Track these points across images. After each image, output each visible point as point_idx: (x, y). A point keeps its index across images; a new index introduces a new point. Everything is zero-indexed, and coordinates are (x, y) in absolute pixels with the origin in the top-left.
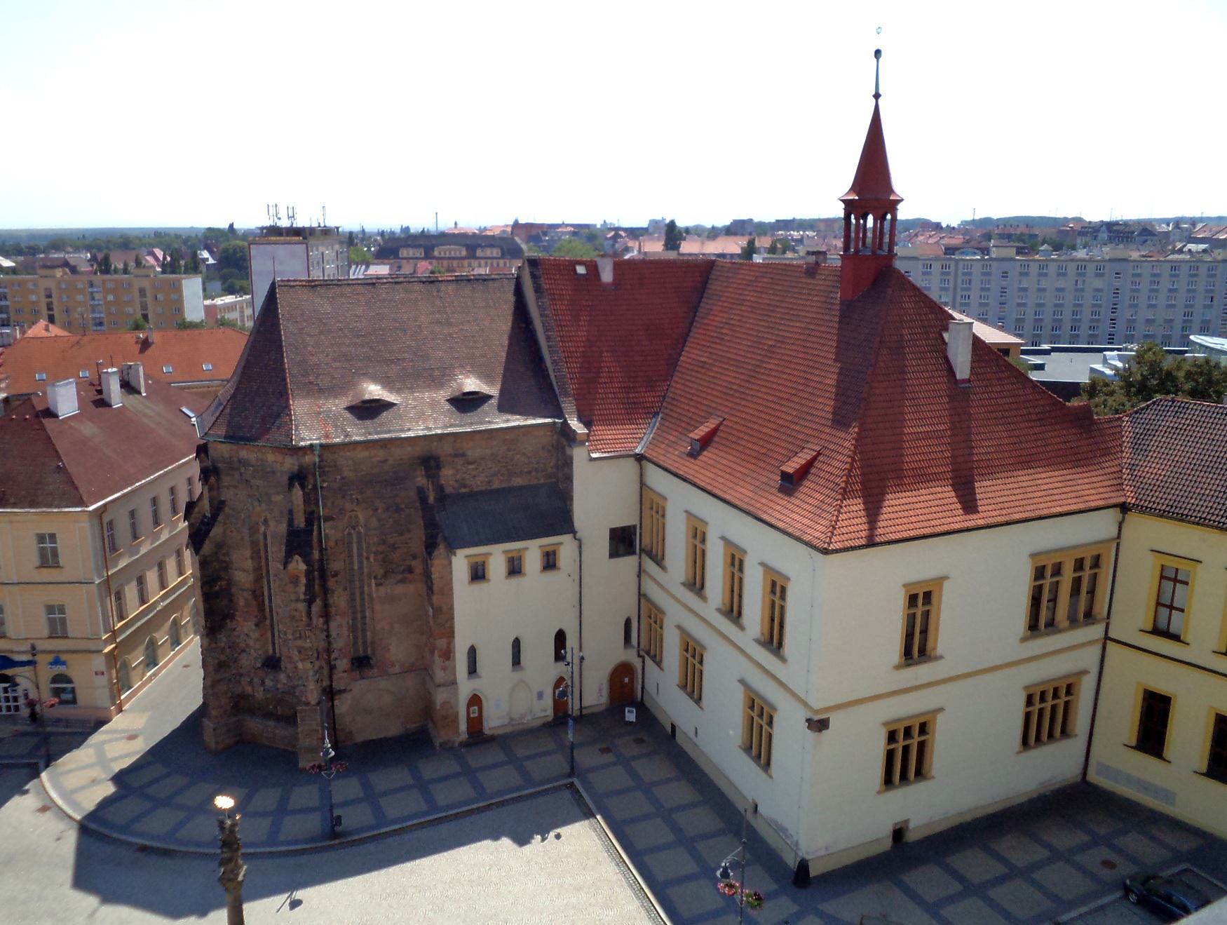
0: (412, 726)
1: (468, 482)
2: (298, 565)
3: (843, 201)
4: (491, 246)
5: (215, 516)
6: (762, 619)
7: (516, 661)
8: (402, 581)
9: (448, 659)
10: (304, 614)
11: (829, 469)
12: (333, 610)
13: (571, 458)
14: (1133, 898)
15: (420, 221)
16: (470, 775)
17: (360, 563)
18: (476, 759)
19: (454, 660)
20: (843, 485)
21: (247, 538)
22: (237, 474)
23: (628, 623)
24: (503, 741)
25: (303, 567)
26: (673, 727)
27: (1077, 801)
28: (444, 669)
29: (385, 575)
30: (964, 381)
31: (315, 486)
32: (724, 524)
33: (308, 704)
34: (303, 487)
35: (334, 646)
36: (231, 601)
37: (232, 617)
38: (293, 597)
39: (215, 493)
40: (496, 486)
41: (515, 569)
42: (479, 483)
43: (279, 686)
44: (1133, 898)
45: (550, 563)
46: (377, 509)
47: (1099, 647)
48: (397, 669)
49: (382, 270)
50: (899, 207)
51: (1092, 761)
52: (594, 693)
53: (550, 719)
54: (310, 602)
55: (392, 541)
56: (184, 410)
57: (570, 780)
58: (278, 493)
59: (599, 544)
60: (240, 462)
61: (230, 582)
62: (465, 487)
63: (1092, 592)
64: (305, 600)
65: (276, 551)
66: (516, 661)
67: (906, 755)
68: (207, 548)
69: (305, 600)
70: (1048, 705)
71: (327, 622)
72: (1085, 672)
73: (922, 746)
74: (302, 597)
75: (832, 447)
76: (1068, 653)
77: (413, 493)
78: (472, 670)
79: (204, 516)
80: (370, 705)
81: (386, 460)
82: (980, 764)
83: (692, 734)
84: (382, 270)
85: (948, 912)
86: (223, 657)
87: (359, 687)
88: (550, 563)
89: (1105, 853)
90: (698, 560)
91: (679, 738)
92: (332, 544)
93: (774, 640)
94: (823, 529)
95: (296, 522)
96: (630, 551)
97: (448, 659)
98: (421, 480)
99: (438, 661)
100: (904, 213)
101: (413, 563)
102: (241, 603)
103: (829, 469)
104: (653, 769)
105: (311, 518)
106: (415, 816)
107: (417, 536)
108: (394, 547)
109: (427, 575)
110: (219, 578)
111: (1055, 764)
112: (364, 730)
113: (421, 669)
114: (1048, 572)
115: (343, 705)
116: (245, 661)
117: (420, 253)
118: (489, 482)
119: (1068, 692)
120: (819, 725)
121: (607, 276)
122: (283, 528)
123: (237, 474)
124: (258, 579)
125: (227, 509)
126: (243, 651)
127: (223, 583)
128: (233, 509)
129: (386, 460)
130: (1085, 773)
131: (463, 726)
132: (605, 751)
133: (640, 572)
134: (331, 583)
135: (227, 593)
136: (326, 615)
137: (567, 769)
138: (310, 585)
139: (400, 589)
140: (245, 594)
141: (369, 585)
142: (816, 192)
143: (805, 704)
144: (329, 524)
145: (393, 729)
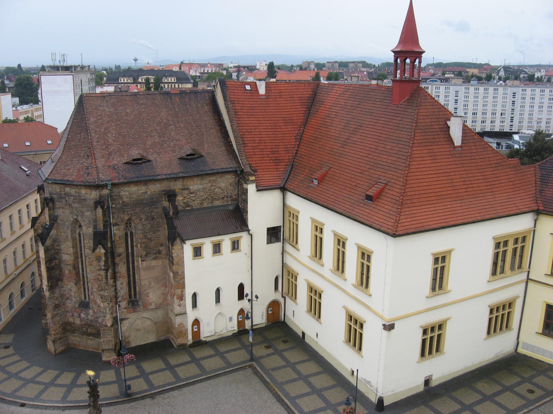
0: (162, 338)
1: (190, 204)
2: (101, 251)
3: (393, 52)
4: (171, 76)
5: (52, 226)
7: (218, 300)
8: (155, 259)
10: (104, 277)
11: (392, 193)
12: (118, 275)
13: (247, 190)
15: (125, 61)
16: (195, 361)
18: (199, 353)
19: (185, 301)
20: (401, 201)
21: (70, 236)
22: (64, 201)
23: (277, 279)
24: (215, 343)
25: (103, 251)
26: (303, 334)
27: (514, 364)
28: (180, 306)
29: (146, 255)
30: (458, 147)
31: (108, 207)
32: (334, 224)
33: (107, 326)
34: (102, 207)
35: (119, 294)
36: (61, 271)
37: (61, 280)
38: (98, 268)
39: (52, 212)
40: (205, 205)
41: (217, 249)
42: (195, 204)
43: (89, 317)
45: (235, 246)
46: (141, 220)
47: (524, 285)
48: (153, 306)
49: (110, 89)
50: (423, 55)
51: (521, 340)
52: (259, 318)
53: (236, 332)
54: (107, 270)
55: (149, 236)
56: (23, 167)
57: (250, 363)
58: (88, 211)
59: (261, 235)
60: (65, 194)
61: (60, 261)
62: (189, 206)
63: (521, 256)
64: (104, 270)
65: (88, 243)
66: (218, 300)
67: (432, 341)
68: (48, 242)
69: (104, 270)
70: (500, 314)
71: (115, 282)
72: (517, 297)
73: (439, 336)
74: (103, 268)
75: (393, 181)
76: (509, 287)
77: (160, 210)
78: (195, 305)
79: (46, 225)
80: (139, 328)
81: (146, 192)
82: (468, 348)
83: (314, 337)
84: (110, 89)
85: (477, 408)
86: (57, 303)
88: (235, 246)
89: (529, 386)
90: (318, 243)
91: (307, 340)
92: (117, 238)
93: (364, 279)
94: (392, 224)
96: (278, 240)
97: (182, 300)
98: (166, 204)
99: (176, 301)
100: (427, 59)
101: (161, 248)
102: (67, 272)
103: (392, 193)
104: (294, 356)
105: (107, 224)
106: (169, 384)
107: (164, 232)
108: (150, 239)
109: (170, 256)
110: (55, 259)
111: (502, 345)
112: (137, 340)
113: (164, 305)
114: (520, 241)
115: (125, 327)
116: (69, 304)
117: (130, 80)
119: (510, 307)
120: (389, 327)
121: (262, 90)
122: (91, 230)
123: (64, 201)
124: (76, 258)
125: (59, 221)
126: (68, 298)
127: (57, 261)
128: (62, 220)
129: (146, 192)
130: (516, 349)
131: (190, 337)
132: (267, 347)
133: (283, 252)
134: (117, 260)
135: (58, 267)
136: (115, 278)
137: (249, 357)
138: (106, 261)
139: (154, 263)
140: (69, 267)
141: (138, 261)
142: (381, 49)
143: (382, 318)
144: (116, 228)
145: (151, 338)
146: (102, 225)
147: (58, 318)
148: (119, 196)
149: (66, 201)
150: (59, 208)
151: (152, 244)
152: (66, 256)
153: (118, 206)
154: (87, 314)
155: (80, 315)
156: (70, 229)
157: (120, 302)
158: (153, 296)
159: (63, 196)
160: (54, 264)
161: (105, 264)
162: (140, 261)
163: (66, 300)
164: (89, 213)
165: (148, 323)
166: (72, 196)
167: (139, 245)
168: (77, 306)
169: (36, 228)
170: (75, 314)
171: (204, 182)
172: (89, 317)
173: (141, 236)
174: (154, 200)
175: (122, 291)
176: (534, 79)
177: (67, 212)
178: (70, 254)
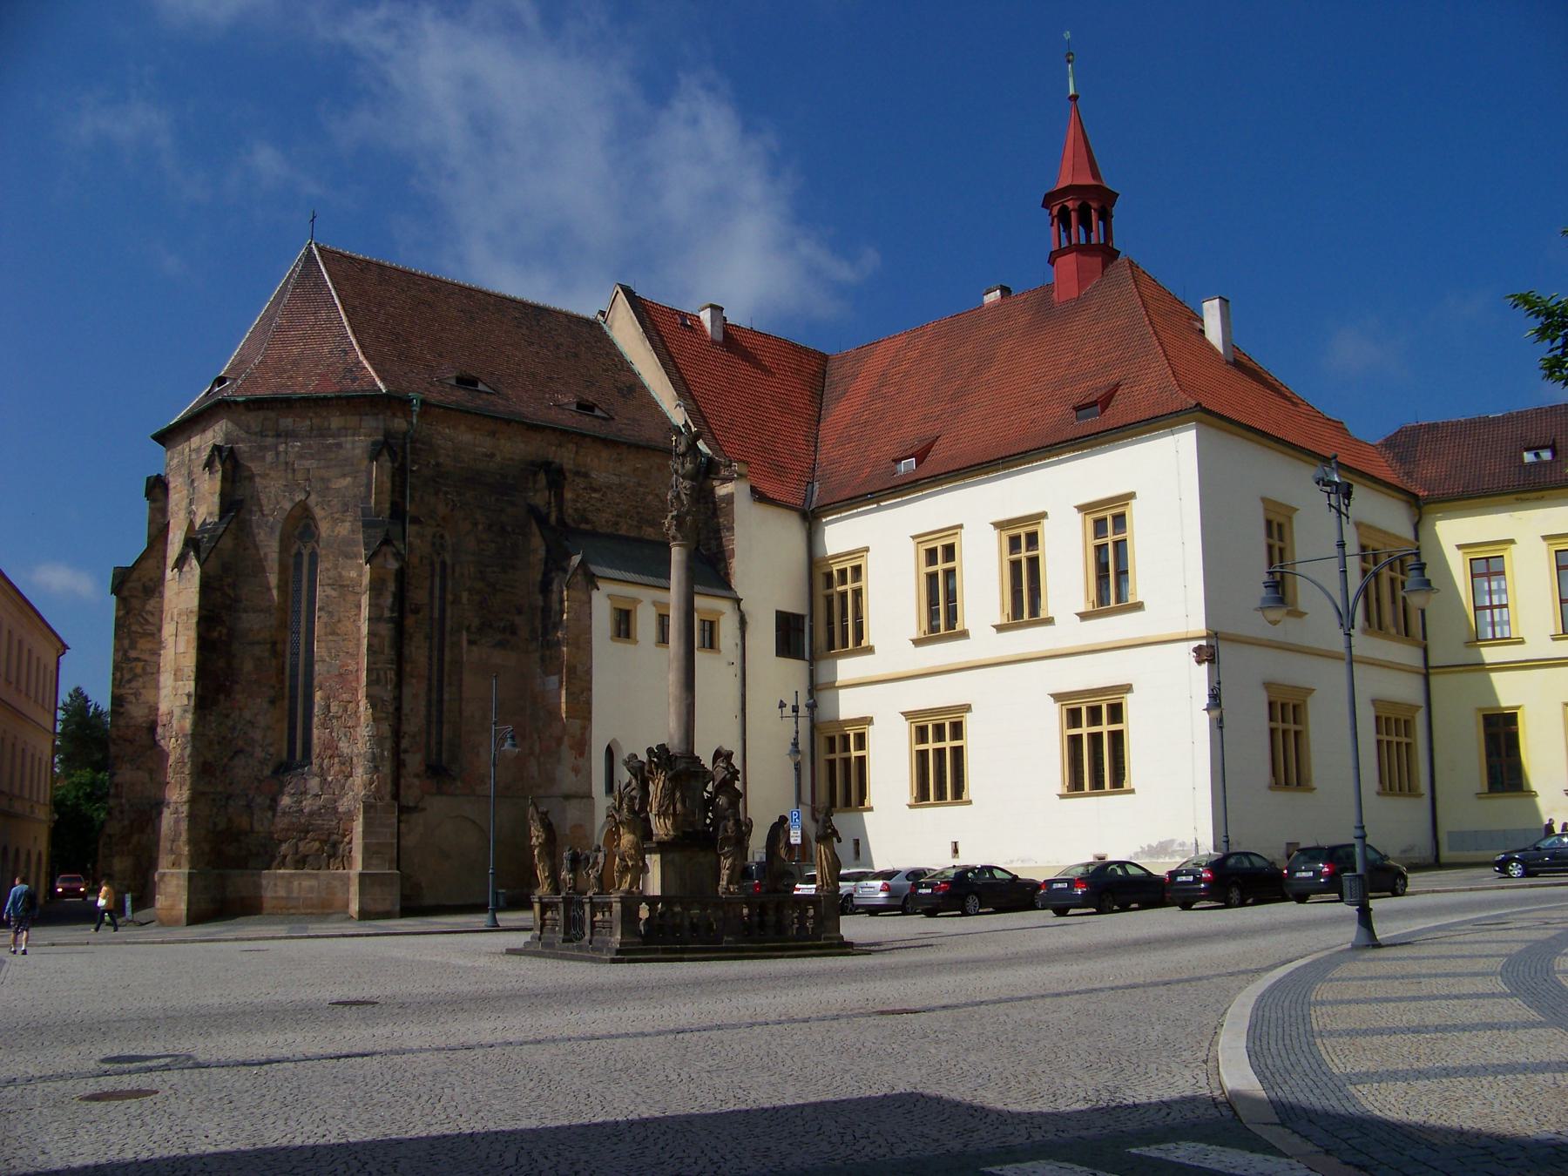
8: (501, 645)
9: (582, 754)
12: (408, 668)
14: (1515, 870)
17: (443, 611)
28: (576, 770)
35: (406, 728)
44: (1515, 870)
46: (476, 524)
51: (1445, 826)
58: (344, 476)
59: (764, 635)
62: (587, 521)
64: (391, 620)
74: (387, 614)
81: (492, 455)
87: (437, 806)
99: (567, 754)
101: (518, 620)
102: (248, 666)
124: (259, 643)
129: (492, 455)
146: (388, 505)
149: (278, 454)
156: (277, 534)
157: (406, 751)
158: (494, 749)
160: (216, 634)
163: (231, 758)
167: (465, 595)
168: (267, 772)
169: (125, 593)
170: (259, 800)
171: (624, 469)
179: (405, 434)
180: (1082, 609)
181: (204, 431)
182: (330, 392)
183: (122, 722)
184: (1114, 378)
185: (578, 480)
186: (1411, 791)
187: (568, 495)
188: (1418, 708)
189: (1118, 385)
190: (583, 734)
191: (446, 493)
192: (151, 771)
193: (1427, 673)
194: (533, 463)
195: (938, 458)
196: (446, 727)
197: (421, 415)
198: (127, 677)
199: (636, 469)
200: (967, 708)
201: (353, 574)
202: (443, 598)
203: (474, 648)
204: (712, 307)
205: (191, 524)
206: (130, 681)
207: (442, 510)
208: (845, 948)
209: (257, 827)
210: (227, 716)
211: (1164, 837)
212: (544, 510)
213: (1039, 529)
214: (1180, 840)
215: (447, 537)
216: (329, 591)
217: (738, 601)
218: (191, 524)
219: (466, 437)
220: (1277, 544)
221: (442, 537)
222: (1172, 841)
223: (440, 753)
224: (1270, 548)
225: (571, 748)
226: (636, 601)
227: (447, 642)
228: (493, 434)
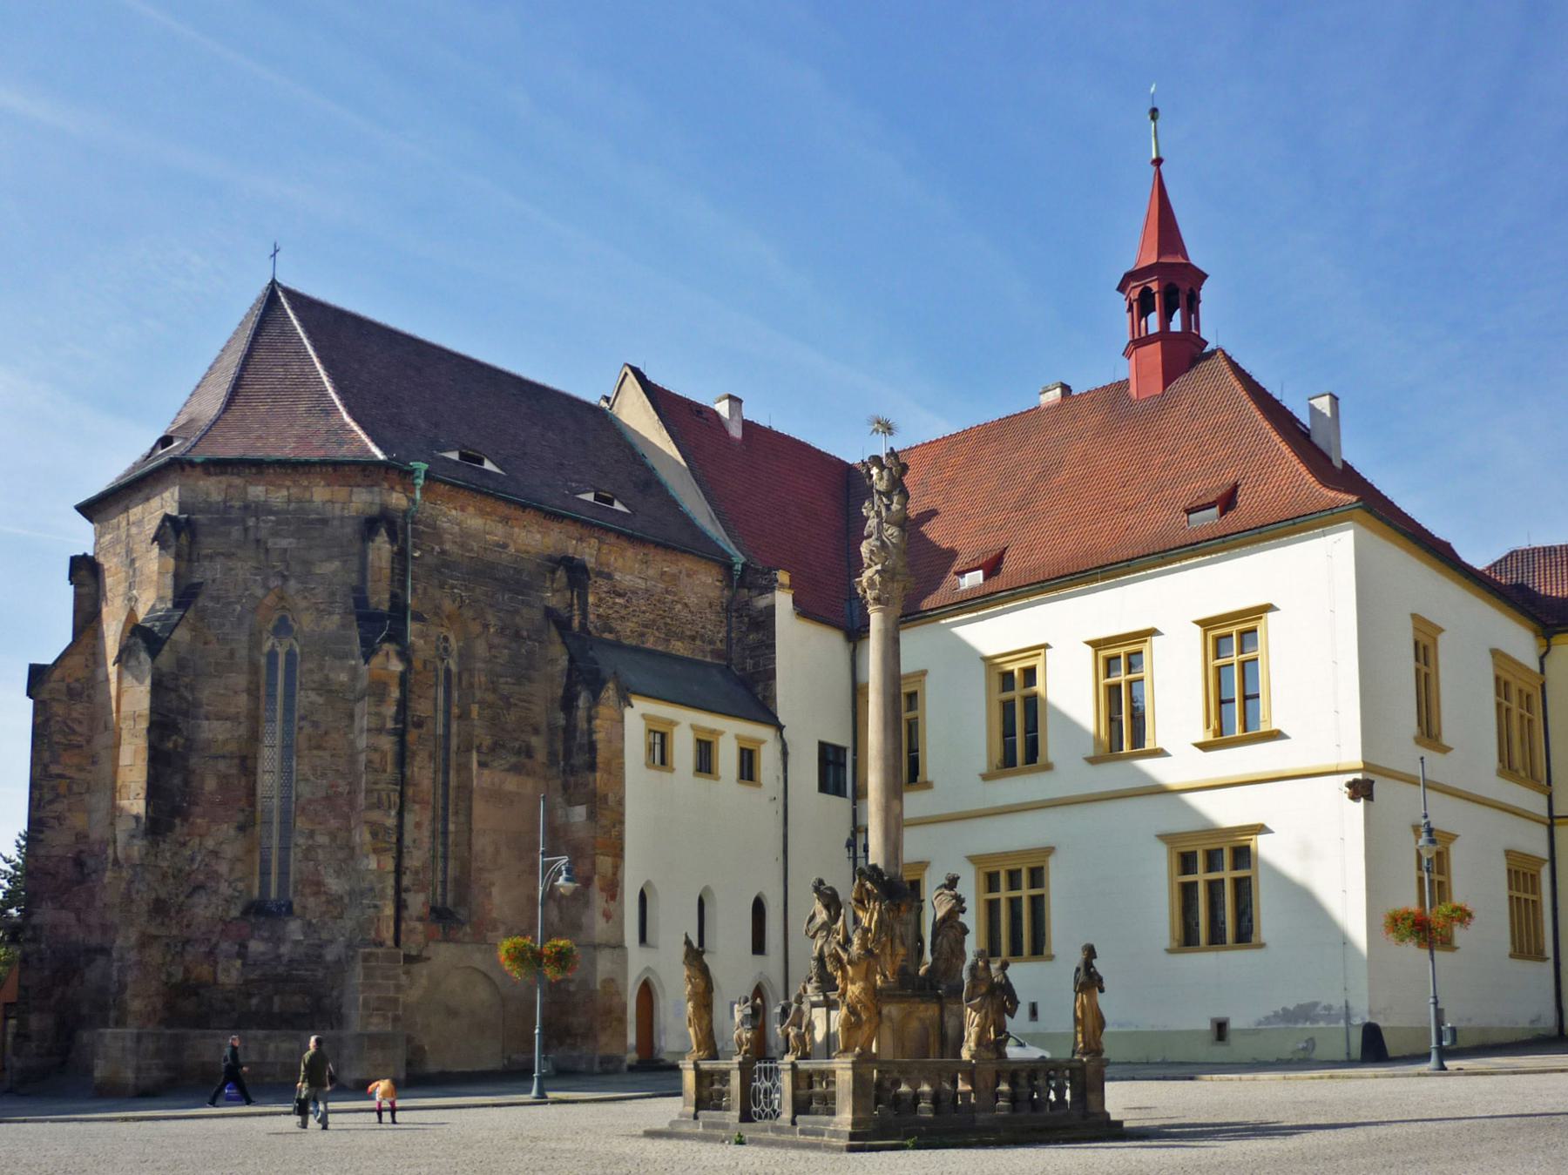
6: (1408, 551)
8: (516, 769)
10: (390, 758)
12: (410, 792)
17: (447, 726)
19: (622, 903)
22: (236, 532)
25: (397, 666)
28: (607, 916)
33: (381, 944)
34: (393, 537)
36: (186, 783)
43: (284, 949)
46: (486, 626)
58: (330, 558)
59: (806, 769)
60: (246, 507)
64: (394, 732)
68: (166, 658)
69: (394, 732)
74: (390, 725)
81: (505, 546)
87: (444, 954)
95: (373, 600)
99: (598, 899)
102: (211, 784)
108: (506, 699)
118: (642, 635)
123: (236, 532)
124: (224, 757)
126: (199, 887)
128: (217, 599)
129: (505, 546)
140: (222, 766)
146: (387, 596)
147: (155, 954)
148: (435, 527)
149: (246, 530)
150: (211, 557)
151: (511, 718)
152: (216, 724)
153: (429, 560)
154: (278, 940)
155: (243, 946)
157: (407, 890)
159: (234, 514)
160: (170, 745)
161: (398, 712)
162: (475, 765)
163: (189, 896)
164: (336, 565)
165: (482, 993)
166: (271, 512)
172: (284, 949)
173: (483, 679)
174: (525, 578)
175: (416, 853)
176: (859, 1055)
177: (243, 568)
178: (234, 718)
179: (405, 513)
180: (1200, 739)
181: (148, 499)
182: (315, 455)
183: (41, 852)
184: (1229, 478)
185: (600, 581)
186: (1539, 956)
187: (591, 599)
188: (1541, 861)
189: (1235, 487)
190: (615, 874)
191: (453, 587)
192: (77, 912)
193: (1551, 821)
194: (550, 559)
195: (1249, 507)
196: (451, 864)
197: (424, 490)
198: (48, 797)
199: (663, 573)
200: (1049, 851)
201: (344, 677)
202: (447, 712)
203: (486, 772)
204: (730, 397)
205: (132, 613)
206: (51, 802)
207: (448, 606)
208: (1114, 1132)
209: (222, 978)
210: (184, 844)
211: (1306, 1000)
212: (564, 613)
213: (1145, 648)
214: (1325, 1003)
215: (452, 639)
216: (313, 696)
217: (780, 728)
218: (132, 613)
219: (474, 522)
220: (1424, 669)
221: (446, 639)
222: (1315, 1004)
223: (444, 895)
224: (1417, 671)
225: (602, 890)
226: (672, 723)
227: (453, 764)
228: (505, 520)
